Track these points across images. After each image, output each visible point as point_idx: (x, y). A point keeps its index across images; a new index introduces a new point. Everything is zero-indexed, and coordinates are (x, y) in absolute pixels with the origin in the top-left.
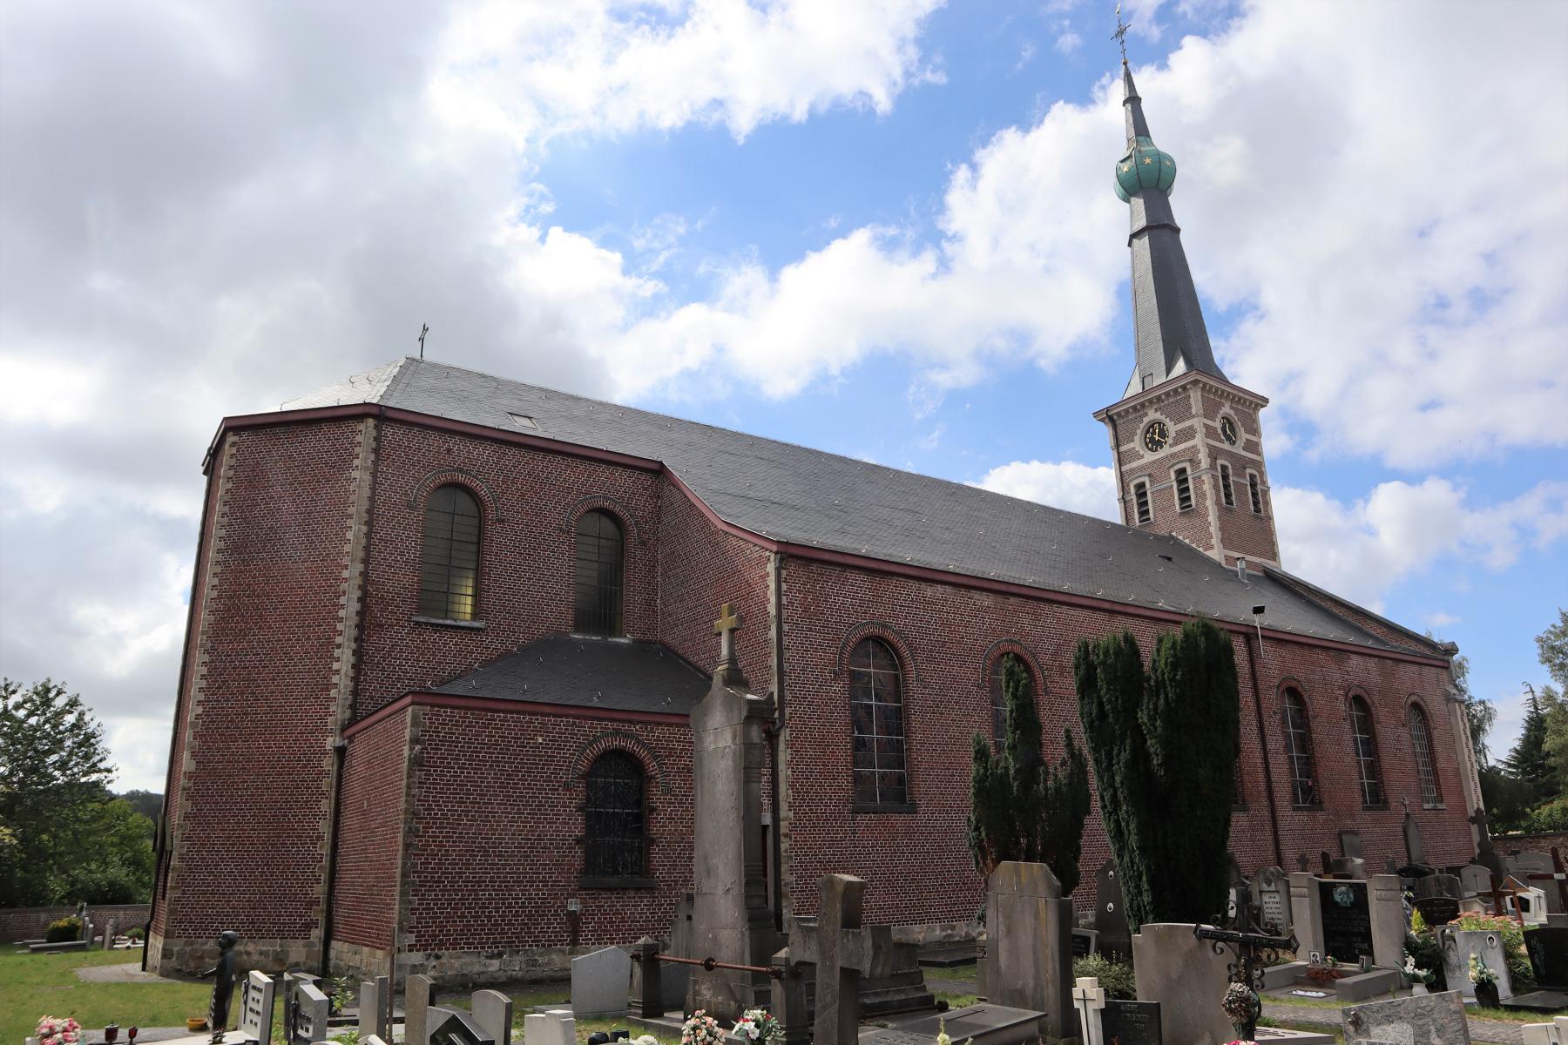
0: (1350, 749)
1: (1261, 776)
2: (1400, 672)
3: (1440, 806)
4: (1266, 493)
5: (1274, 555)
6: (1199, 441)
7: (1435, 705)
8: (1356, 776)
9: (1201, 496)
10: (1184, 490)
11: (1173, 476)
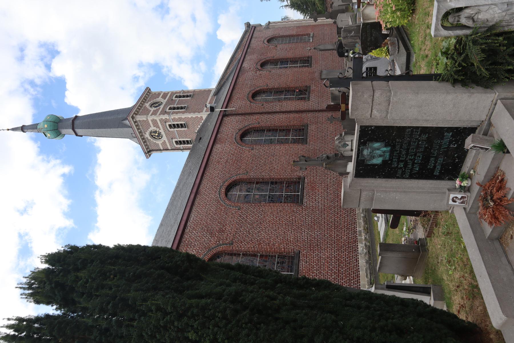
0: (283, 71)
1: (292, 115)
2: (257, 47)
3: (312, 35)
4: (184, 92)
5: (210, 91)
6: (157, 118)
7: (270, 34)
8: (296, 69)
9: (180, 119)
10: (178, 126)
11: (172, 130)
